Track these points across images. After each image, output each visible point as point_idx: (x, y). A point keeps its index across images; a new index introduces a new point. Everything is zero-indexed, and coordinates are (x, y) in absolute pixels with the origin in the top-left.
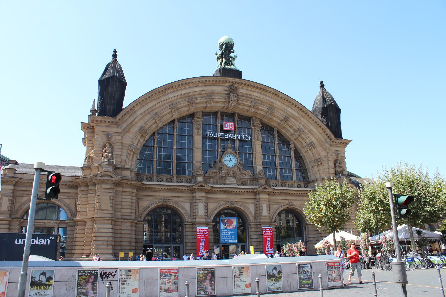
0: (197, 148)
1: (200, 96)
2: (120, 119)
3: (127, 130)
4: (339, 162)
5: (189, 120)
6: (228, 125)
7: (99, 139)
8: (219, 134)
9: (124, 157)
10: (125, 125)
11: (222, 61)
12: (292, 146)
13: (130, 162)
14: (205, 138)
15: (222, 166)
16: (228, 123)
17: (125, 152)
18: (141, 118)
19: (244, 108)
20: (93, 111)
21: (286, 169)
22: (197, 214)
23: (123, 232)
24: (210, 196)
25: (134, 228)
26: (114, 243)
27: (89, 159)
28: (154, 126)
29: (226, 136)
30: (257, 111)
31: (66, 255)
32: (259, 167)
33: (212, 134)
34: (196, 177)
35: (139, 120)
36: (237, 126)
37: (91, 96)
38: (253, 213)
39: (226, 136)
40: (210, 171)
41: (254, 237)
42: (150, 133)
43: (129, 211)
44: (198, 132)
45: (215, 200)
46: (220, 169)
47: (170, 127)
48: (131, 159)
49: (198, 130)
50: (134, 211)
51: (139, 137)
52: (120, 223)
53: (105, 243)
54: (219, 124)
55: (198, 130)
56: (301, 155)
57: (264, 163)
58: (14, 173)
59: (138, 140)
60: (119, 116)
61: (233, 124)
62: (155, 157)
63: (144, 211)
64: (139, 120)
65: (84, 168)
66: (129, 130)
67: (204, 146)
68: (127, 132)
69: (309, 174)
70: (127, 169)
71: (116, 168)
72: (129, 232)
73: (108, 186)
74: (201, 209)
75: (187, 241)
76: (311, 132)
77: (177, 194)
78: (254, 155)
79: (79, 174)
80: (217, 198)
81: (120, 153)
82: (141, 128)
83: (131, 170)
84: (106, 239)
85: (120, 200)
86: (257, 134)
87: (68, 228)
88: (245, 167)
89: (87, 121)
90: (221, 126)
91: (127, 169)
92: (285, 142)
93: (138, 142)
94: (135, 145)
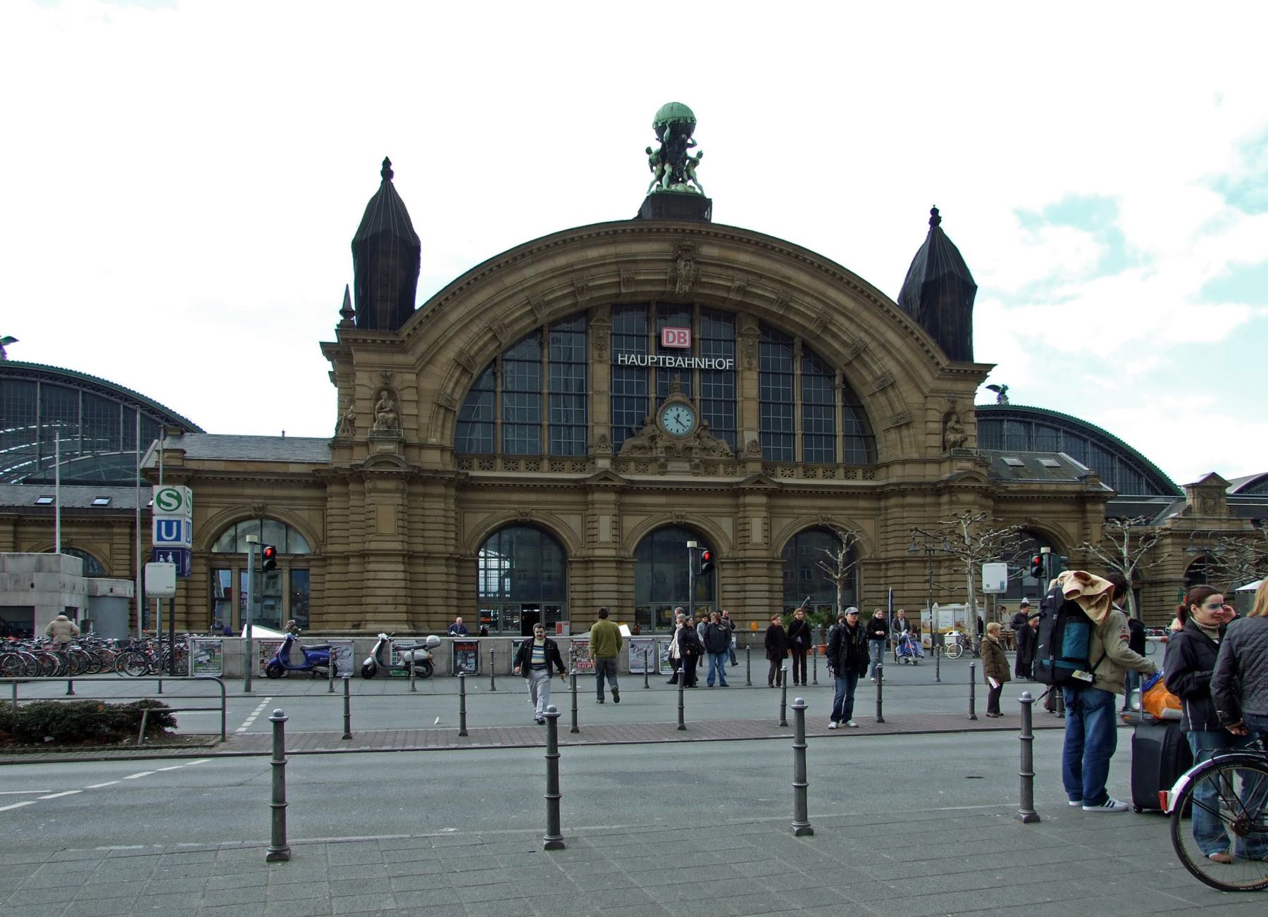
0: (599, 393)
1: (602, 270)
2: (409, 335)
3: (428, 359)
4: (954, 418)
5: (579, 325)
6: (676, 336)
7: (366, 382)
8: (650, 359)
9: (425, 420)
10: (422, 348)
11: (663, 172)
12: (838, 381)
13: (439, 429)
14: (617, 368)
15: (658, 432)
16: (676, 331)
17: (426, 411)
18: (460, 330)
19: (720, 285)
20: (345, 312)
21: (819, 436)
22: (595, 538)
23: (430, 578)
24: (628, 499)
25: (454, 570)
26: (409, 601)
27: (345, 423)
28: (492, 347)
29: (670, 361)
30: (749, 300)
31: (311, 625)
32: (750, 436)
33: (634, 359)
34: (594, 458)
35: (456, 334)
36: (697, 336)
37: (338, 276)
38: (731, 537)
39: (670, 361)
40: (628, 443)
41: (730, 588)
42: (481, 361)
43: (442, 534)
44: (600, 356)
45: (639, 510)
46: (653, 438)
47: (533, 342)
48: (440, 422)
49: (601, 349)
50: (453, 535)
51: (457, 374)
52: (422, 561)
53: (390, 600)
54: (653, 334)
55: (601, 349)
56: (863, 402)
57: (764, 423)
58: (184, 459)
59: (454, 380)
60: (406, 329)
61: (687, 332)
62: (499, 415)
63: (478, 535)
64: (456, 334)
65: (334, 444)
66: (433, 357)
67: (616, 387)
68: (428, 363)
69: (879, 447)
70: (433, 447)
71: (405, 445)
72: (444, 578)
73: (390, 485)
74: (605, 528)
75: (575, 595)
76: (886, 347)
77: (550, 497)
78: (739, 406)
79: (323, 456)
80: (645, 505)
81: (415, 412)
82: (461, 353)
83: (442, 449)
84: (392, 592)
85: (420, 511)
86: (750, 356)
87: (312, 571)
88: (717, 433)
89: (333, 338)
90: (659, 338)
91: (433, 447)
92: (820, 366)
93: (456, 384)
94: (449, 391)
